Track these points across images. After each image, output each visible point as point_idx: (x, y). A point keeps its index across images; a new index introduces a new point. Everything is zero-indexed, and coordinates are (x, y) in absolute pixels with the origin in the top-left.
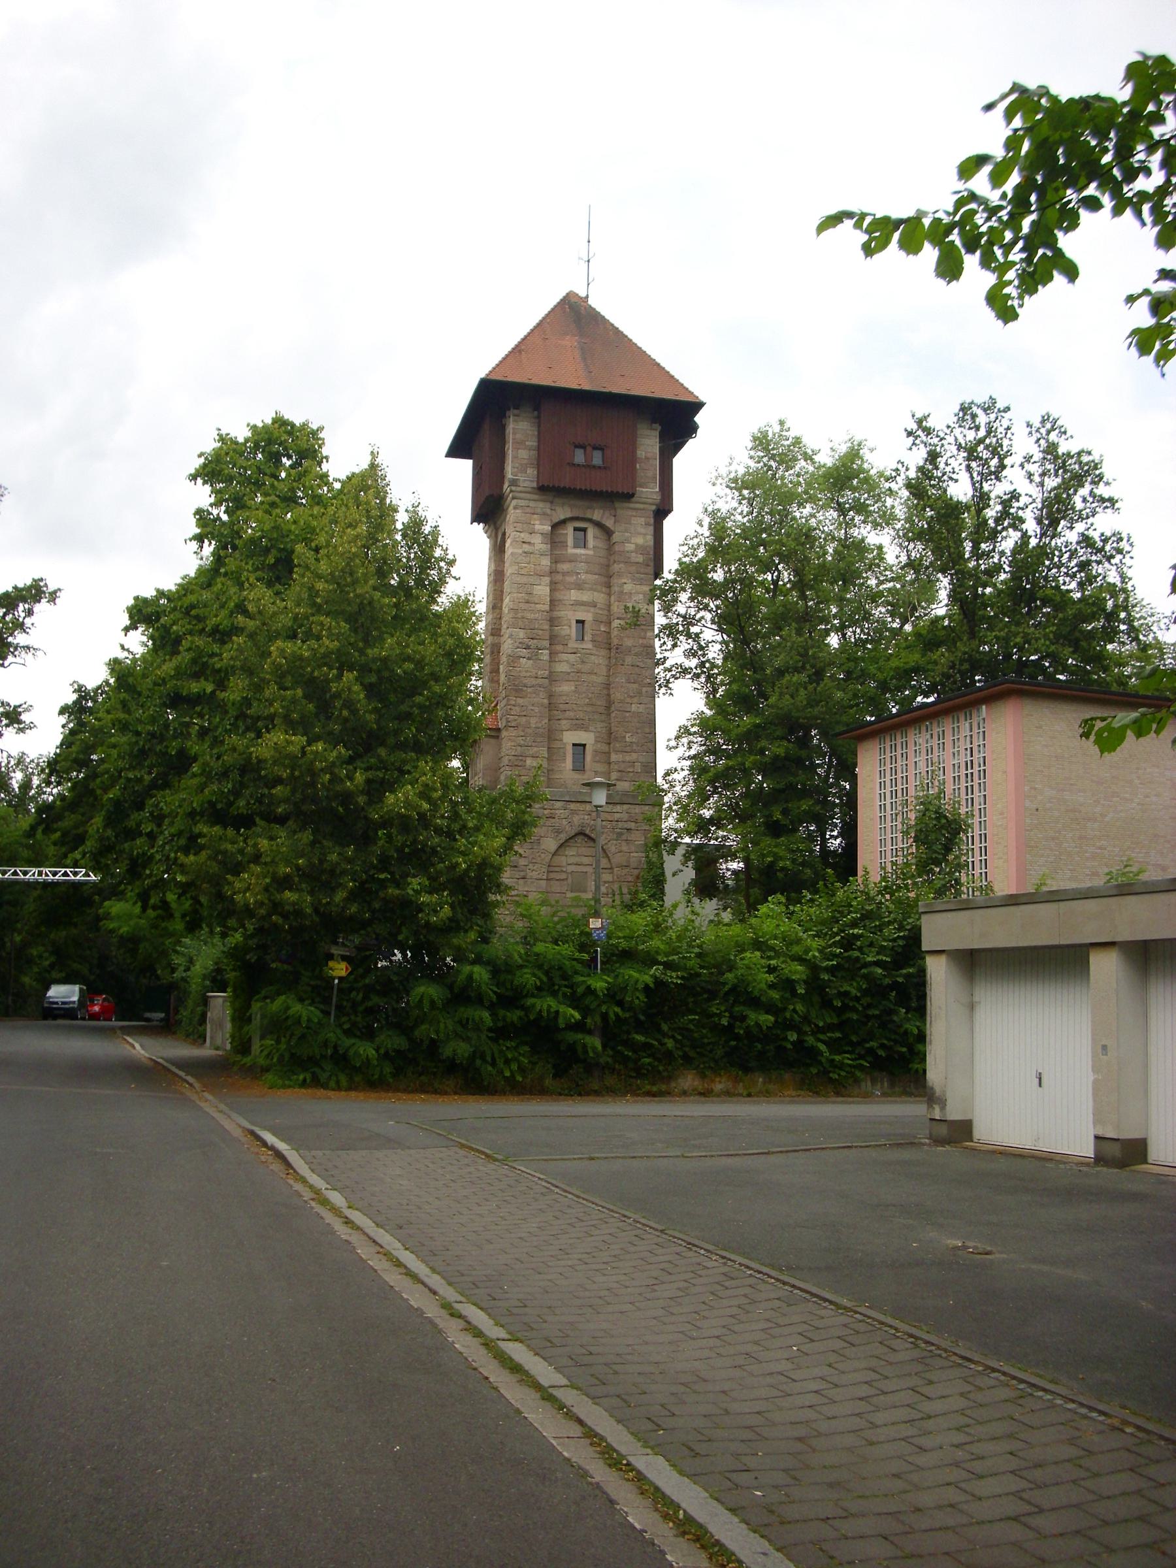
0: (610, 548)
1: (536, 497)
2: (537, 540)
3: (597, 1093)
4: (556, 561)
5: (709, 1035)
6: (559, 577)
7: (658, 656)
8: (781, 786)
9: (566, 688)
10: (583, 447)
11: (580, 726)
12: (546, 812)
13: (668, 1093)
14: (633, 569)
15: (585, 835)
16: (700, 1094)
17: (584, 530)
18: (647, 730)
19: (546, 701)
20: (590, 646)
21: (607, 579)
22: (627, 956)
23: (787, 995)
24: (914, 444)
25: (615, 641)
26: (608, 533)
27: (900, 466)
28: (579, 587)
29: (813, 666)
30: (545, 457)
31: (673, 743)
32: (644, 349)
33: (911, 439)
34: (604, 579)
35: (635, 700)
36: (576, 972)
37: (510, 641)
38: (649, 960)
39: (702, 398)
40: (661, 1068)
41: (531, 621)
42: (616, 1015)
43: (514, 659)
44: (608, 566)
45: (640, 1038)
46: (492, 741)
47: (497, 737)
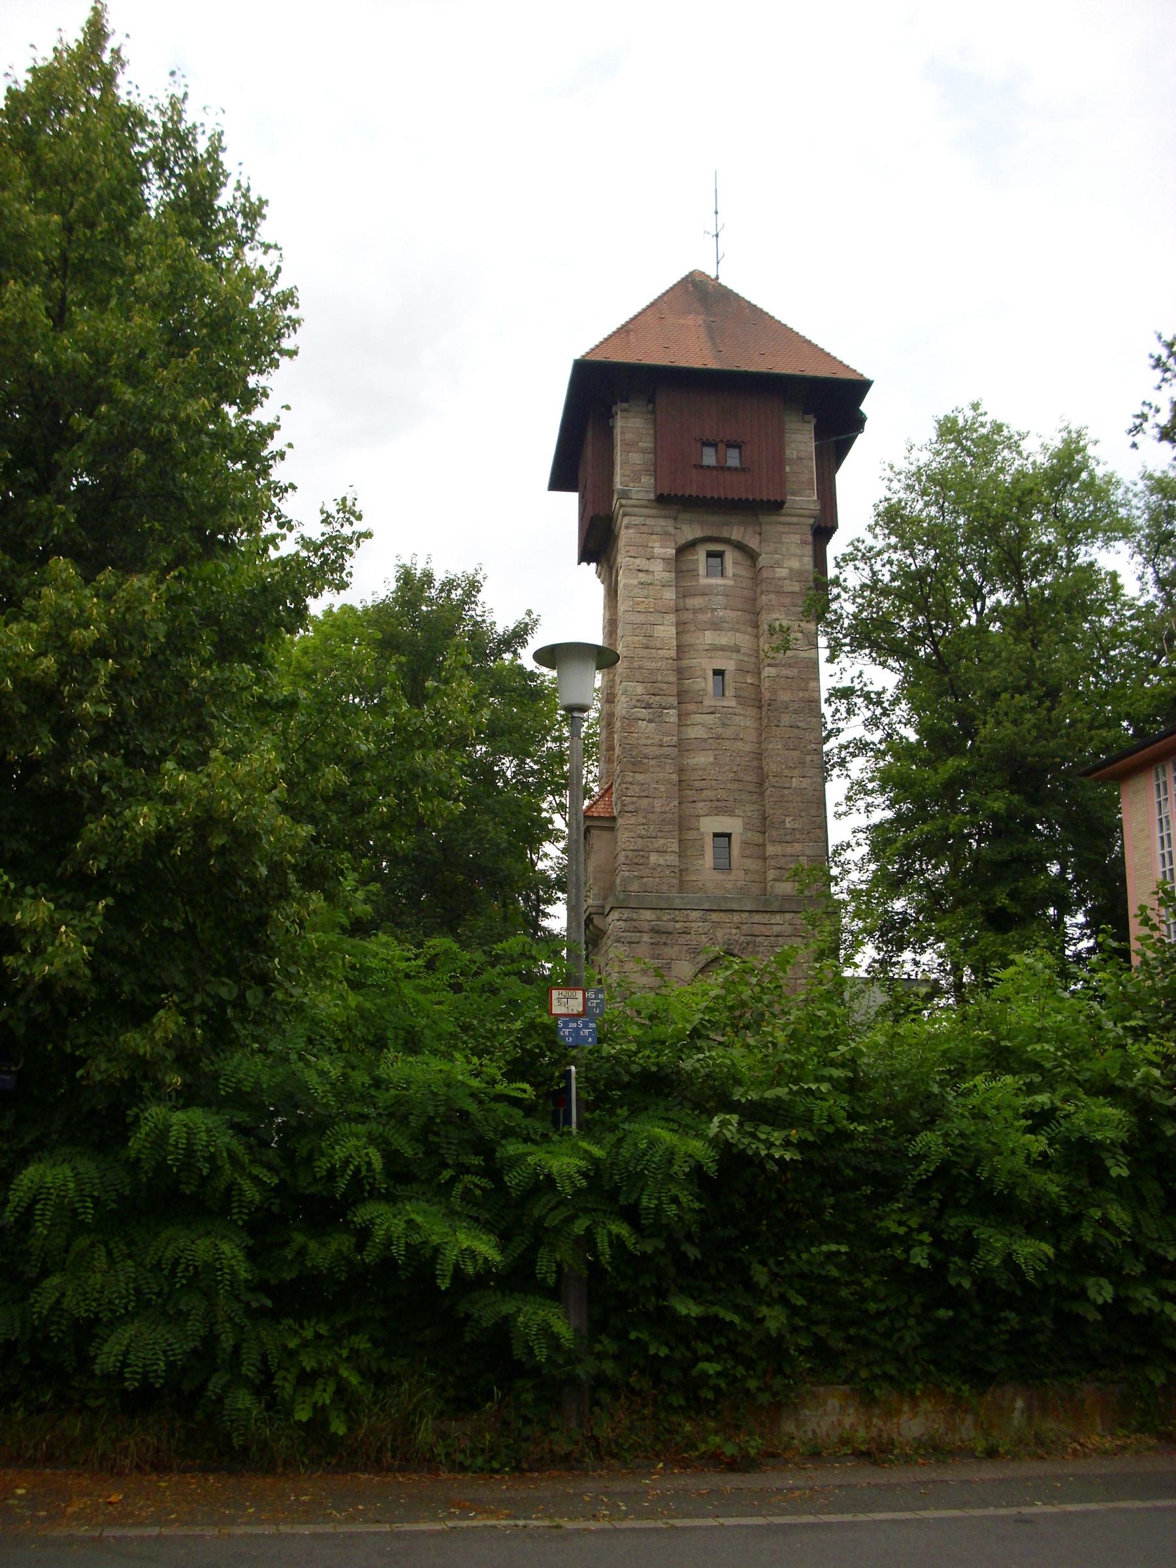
0: (756, 577)
2: (657, 567)
3: (568, 1463)
4: (683, 595)
5: (882, 1291)
6: (688, 616)
7: (829, 726)
8: (1005, 856)
9: (702, 759)
10: (713, 445)
11: (721, 808)
12: (678, 925)
13: (772, 1457)
14: (787, 601)
16: (859, 1454)
17: (720, 555)
18: (813, 812)
19: (675, 777)
20: (733, 703)
21: (753, 613)
22: (654, 1087)
23: (1084, 1183)
24: (1164, 380)
25: (767, 695)
26: (751, 556)
27: (1146, 410)
28: (716, 626)
29: (1043, 683)
30: (667, 458)
31: (843, 809)
32: (790, 325)
33: (1158, 374)
34: (748, 617)
35: (796, 772)
36: (509, 1133)
37: (624, 699)
38: (715, 1096)
39: (868, 375)
40: (752, 1384)
41: (652, 671)
42: (617, 1243)
43: (631, 721)
44: (755, 600)
45: (687, 1308)
46: (606, 835)
47: (612, 829)
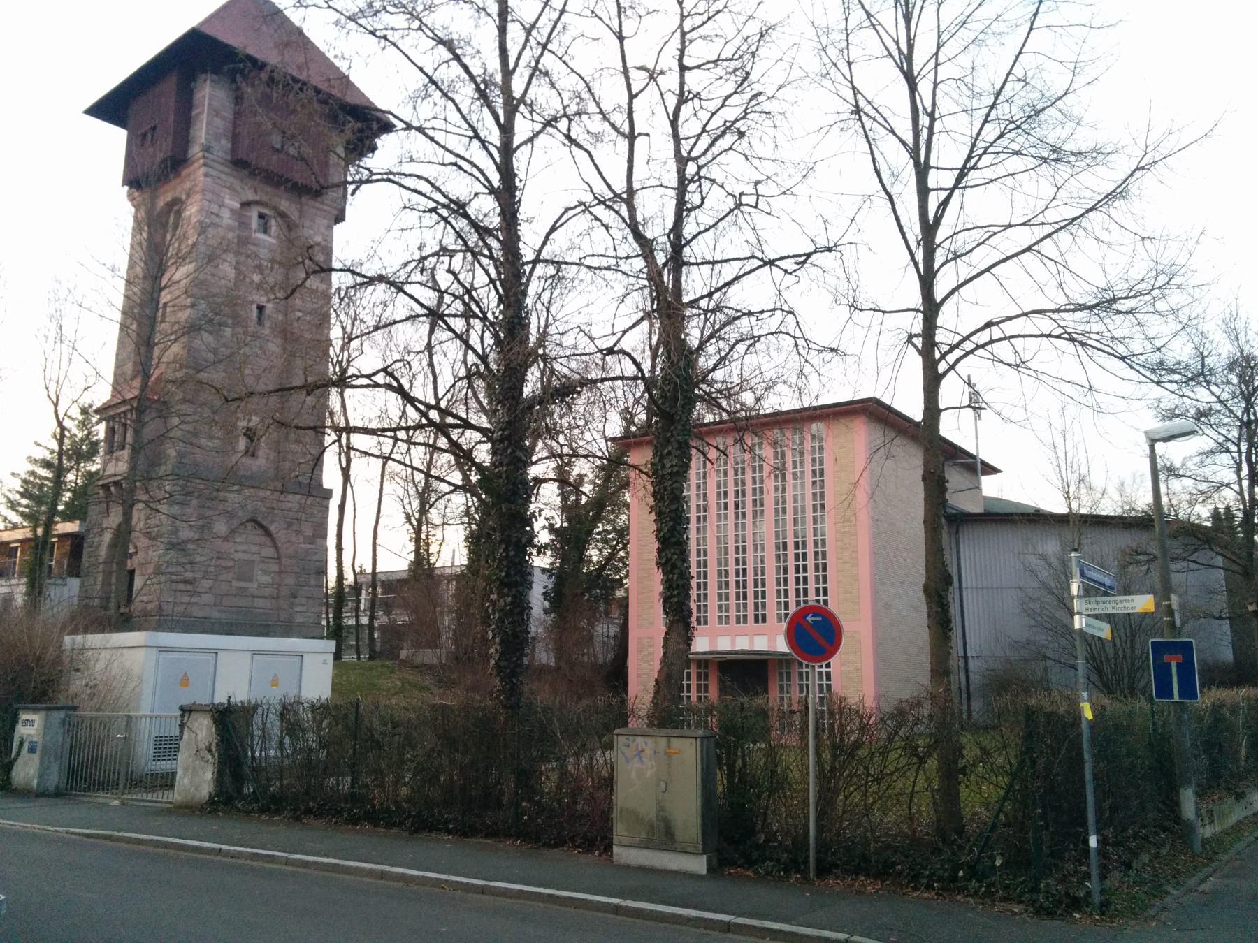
1: (226, 170)
2: (226, 214)
15: (255, 521)
